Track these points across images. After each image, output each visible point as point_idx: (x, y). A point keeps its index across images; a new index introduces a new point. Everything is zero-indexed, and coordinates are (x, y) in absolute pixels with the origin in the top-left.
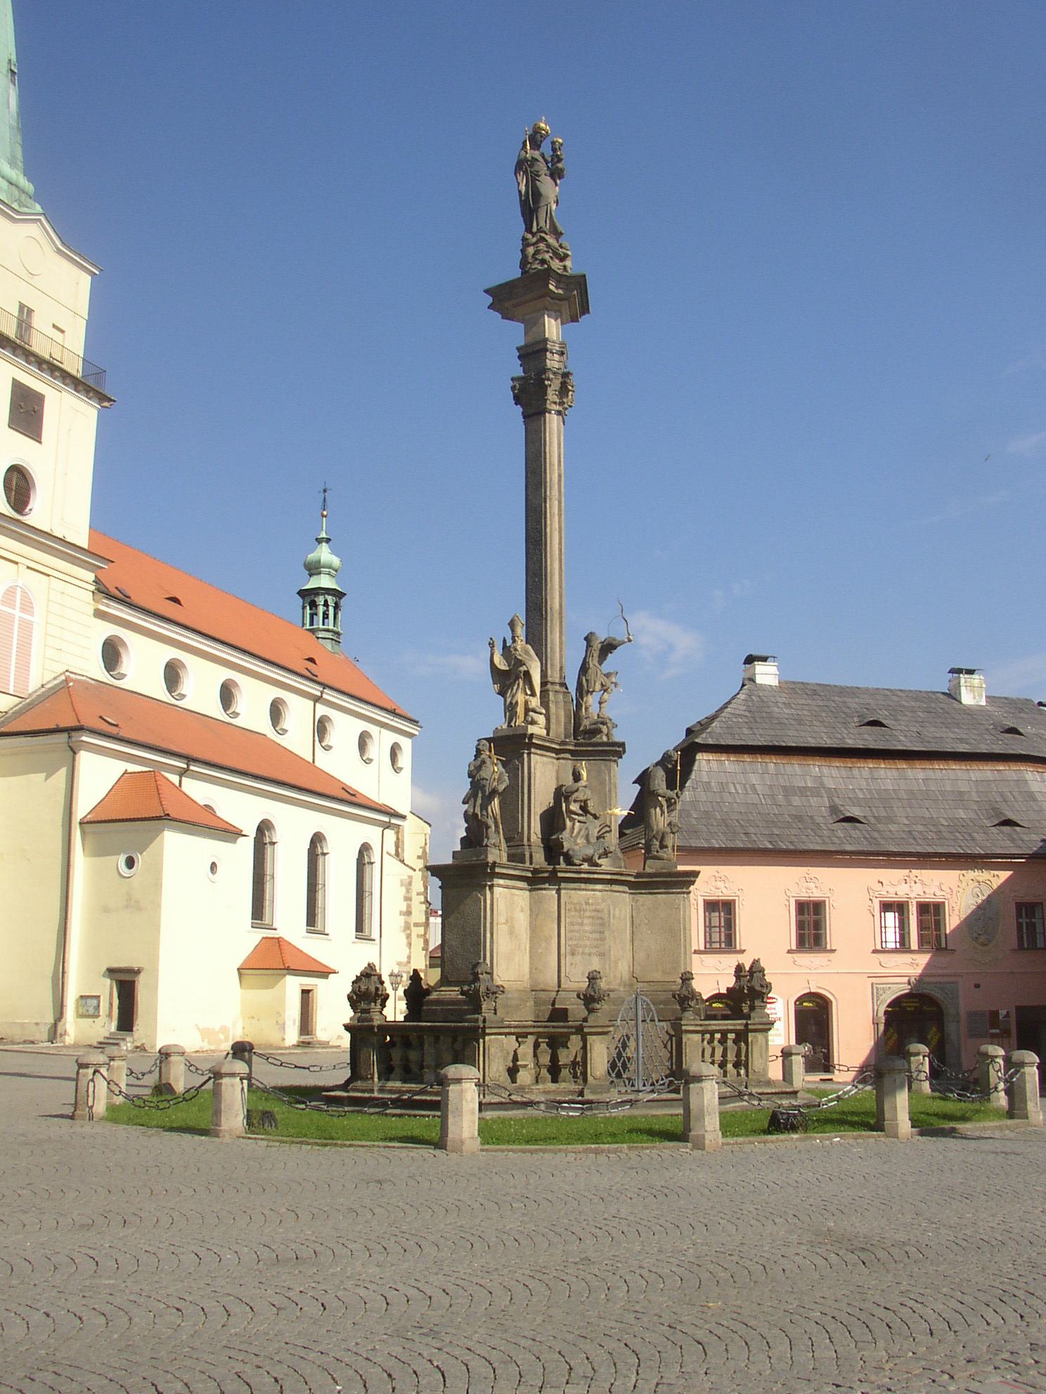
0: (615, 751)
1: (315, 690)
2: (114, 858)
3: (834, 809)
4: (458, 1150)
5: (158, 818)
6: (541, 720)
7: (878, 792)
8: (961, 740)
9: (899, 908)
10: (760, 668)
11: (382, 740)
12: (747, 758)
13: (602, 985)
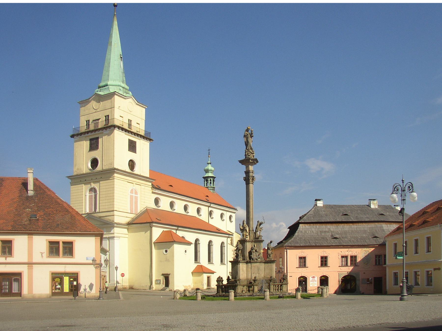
0: (262, 241)
2: (162, 250)
4: (231, 300)
5: (173, 242)
6: (249, 237)
8: (367, 218)
9: (346, 257)
10: (318, 202)
11: (227, 215)
12: (312, 225)
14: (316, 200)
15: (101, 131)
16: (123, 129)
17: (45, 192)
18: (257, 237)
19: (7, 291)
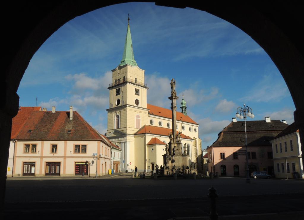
1: (182, 122)
10: (234, 119)
13: (175, 166)
14: (266, 117)
16: (131, 83)
17: (78, 118)
18: (178, 141)
19: (54, 173)
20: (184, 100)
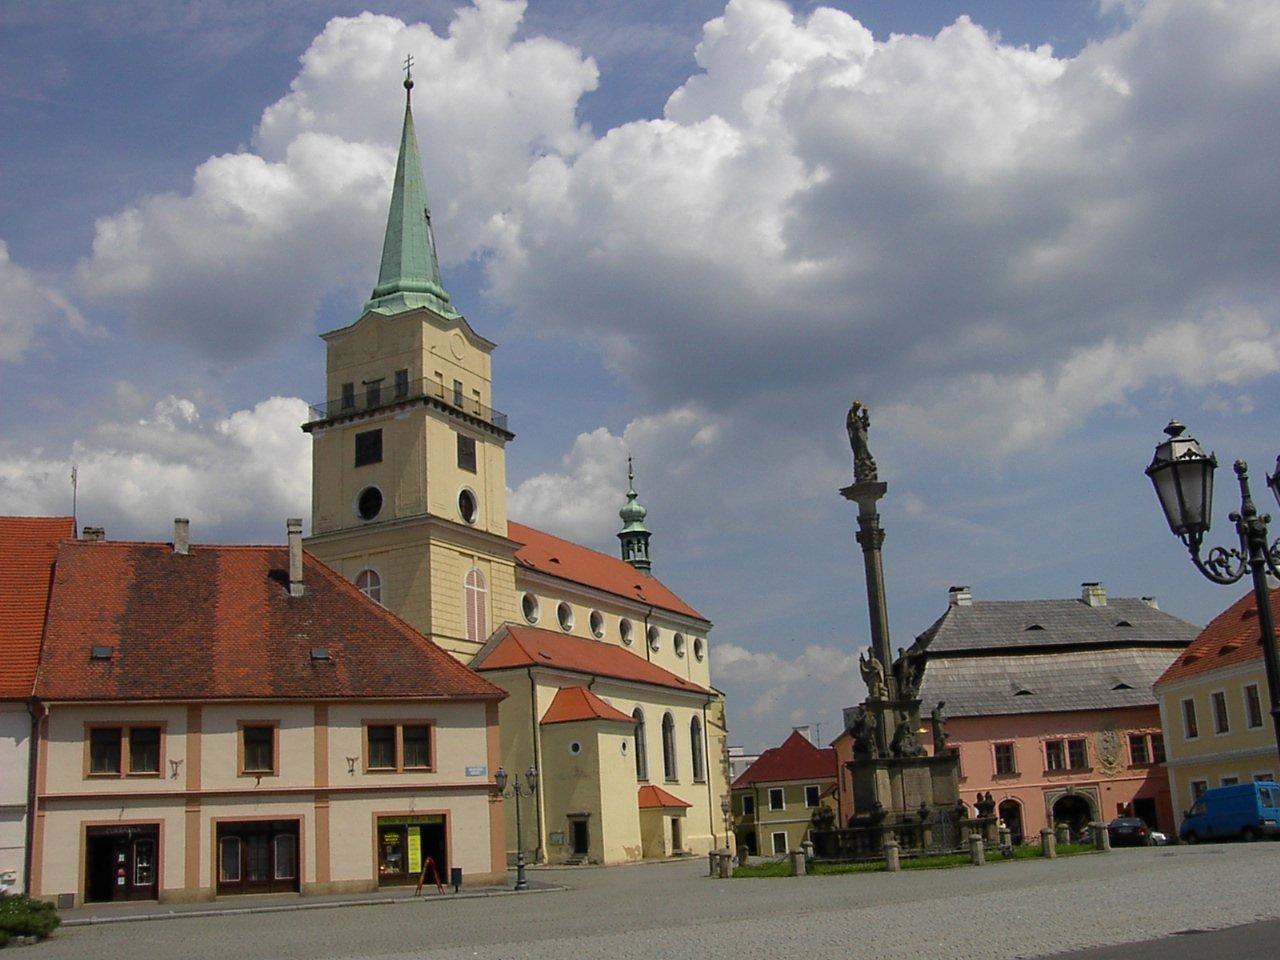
3: (1013, 686)
7: (1041, 672)
14: (953, 589)
15: (388, 414)
20: (634, 502)
